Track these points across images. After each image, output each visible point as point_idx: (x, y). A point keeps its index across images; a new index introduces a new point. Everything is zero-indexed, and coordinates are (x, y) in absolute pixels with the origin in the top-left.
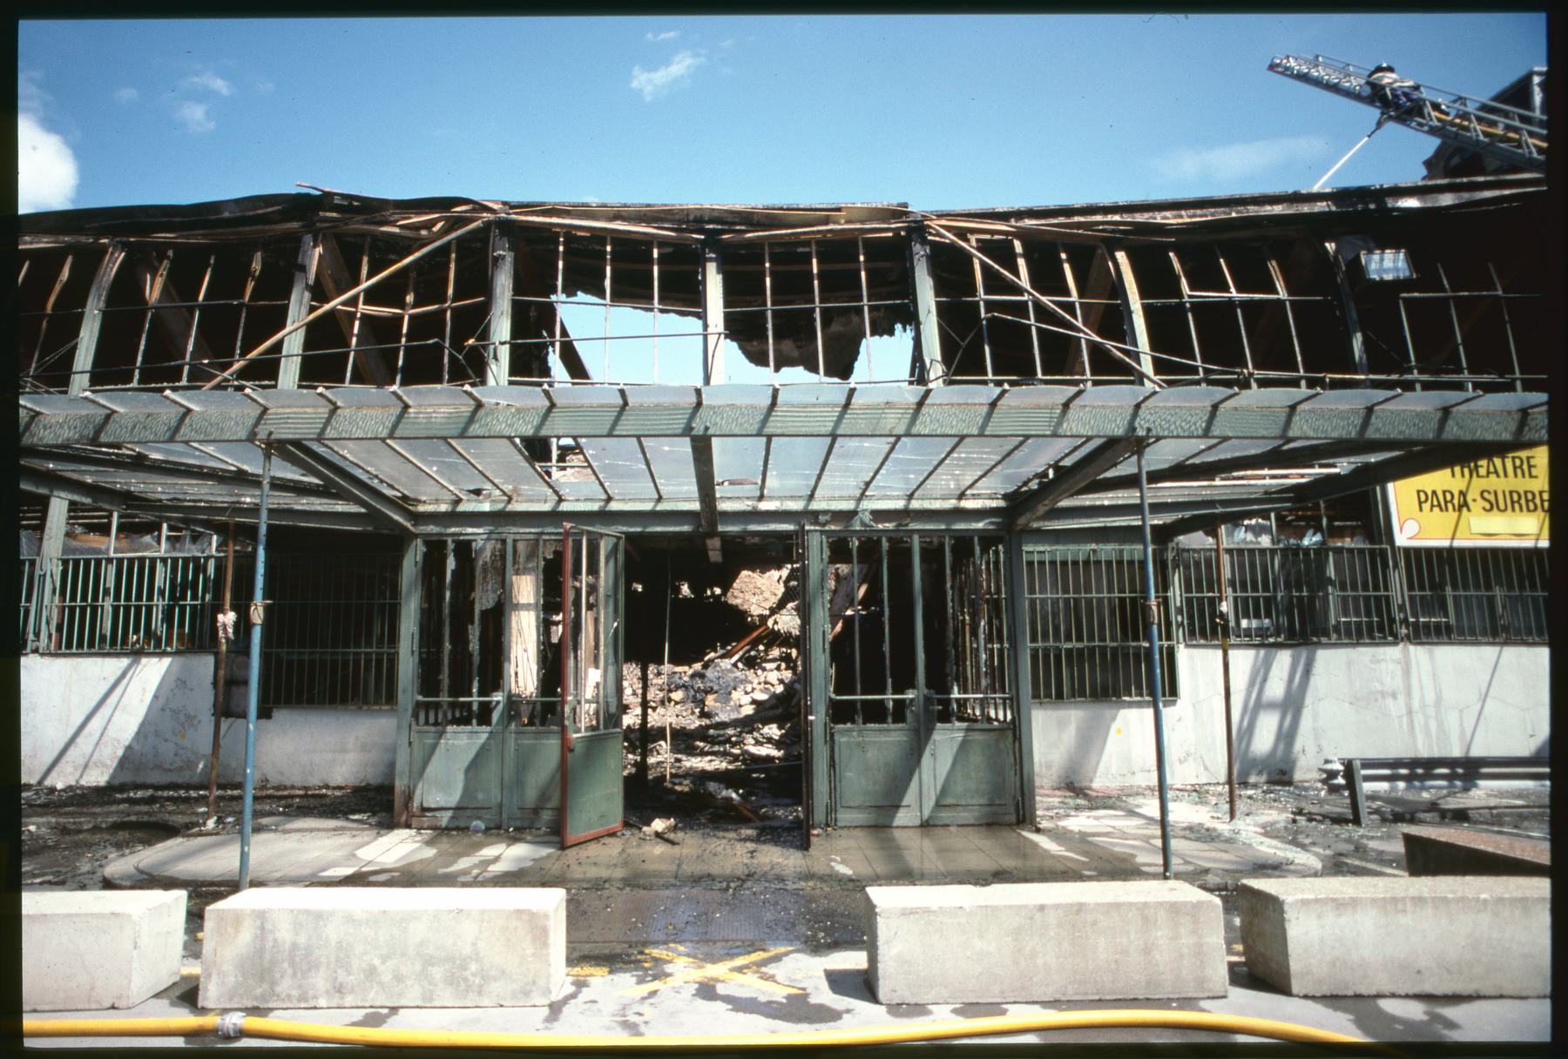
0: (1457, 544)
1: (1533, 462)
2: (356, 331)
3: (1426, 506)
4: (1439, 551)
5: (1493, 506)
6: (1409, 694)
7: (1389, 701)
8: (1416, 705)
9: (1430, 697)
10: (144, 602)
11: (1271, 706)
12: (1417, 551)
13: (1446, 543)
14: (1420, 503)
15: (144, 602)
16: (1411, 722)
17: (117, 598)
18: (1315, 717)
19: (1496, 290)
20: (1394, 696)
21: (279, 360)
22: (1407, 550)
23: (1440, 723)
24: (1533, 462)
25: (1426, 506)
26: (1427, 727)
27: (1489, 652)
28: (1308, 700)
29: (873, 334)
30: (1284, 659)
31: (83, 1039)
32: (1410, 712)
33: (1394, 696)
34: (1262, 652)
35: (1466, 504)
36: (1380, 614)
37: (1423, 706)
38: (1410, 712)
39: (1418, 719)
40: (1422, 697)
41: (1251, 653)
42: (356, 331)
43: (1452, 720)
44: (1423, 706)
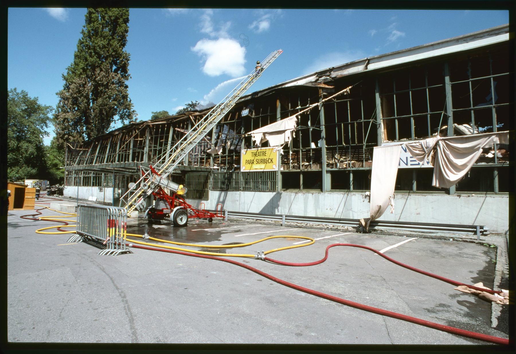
0: (251, 171)
1: (266, 152)
2: (371, 144)
3: (247, 163)
4: (247, 172)
5: (258, 163)
6: (240, 200)
7: (237, 202)
8: (241, 203)
9: (243, 201)
10: (274, 181)
11: (220, 202)
12: (244, 172)
13: (248, 171)
14: (246, 162)
15: (274, 181)
16: (240, 206)
17: (235, 180)
18: (226, 204)
19: (261, 115)
20: (238, 201)
21: (133, 148)
22: (242, 172)
23: (244, 206)
24: (266, 152)
25: (247, 163)
26: (242, 208)
27: (253, 193)
28: (226, 201)
29: (391, 137)
30: (223, 193)
31: (413, 232)
32: (240, 204)
33: (238, 201)
34: (220, 192)
35: (253, 163)
36: (237, 185)
37: (242, 203)
38: (240, 204)
39: (241, 205)
40: (242, 202)
41: (219, 192)
42: (371, 144)
43: (246, 206)
44: (242, 203)
